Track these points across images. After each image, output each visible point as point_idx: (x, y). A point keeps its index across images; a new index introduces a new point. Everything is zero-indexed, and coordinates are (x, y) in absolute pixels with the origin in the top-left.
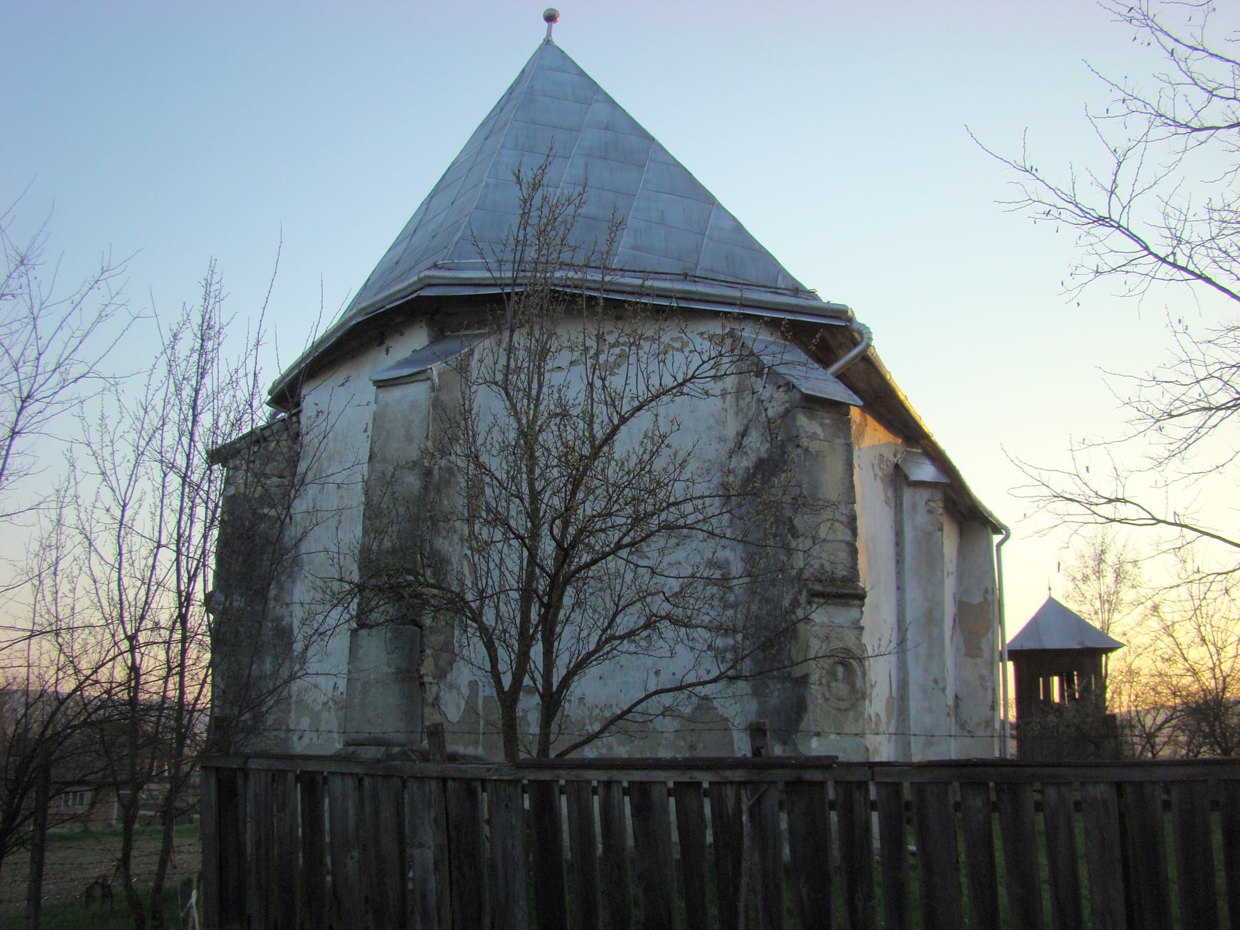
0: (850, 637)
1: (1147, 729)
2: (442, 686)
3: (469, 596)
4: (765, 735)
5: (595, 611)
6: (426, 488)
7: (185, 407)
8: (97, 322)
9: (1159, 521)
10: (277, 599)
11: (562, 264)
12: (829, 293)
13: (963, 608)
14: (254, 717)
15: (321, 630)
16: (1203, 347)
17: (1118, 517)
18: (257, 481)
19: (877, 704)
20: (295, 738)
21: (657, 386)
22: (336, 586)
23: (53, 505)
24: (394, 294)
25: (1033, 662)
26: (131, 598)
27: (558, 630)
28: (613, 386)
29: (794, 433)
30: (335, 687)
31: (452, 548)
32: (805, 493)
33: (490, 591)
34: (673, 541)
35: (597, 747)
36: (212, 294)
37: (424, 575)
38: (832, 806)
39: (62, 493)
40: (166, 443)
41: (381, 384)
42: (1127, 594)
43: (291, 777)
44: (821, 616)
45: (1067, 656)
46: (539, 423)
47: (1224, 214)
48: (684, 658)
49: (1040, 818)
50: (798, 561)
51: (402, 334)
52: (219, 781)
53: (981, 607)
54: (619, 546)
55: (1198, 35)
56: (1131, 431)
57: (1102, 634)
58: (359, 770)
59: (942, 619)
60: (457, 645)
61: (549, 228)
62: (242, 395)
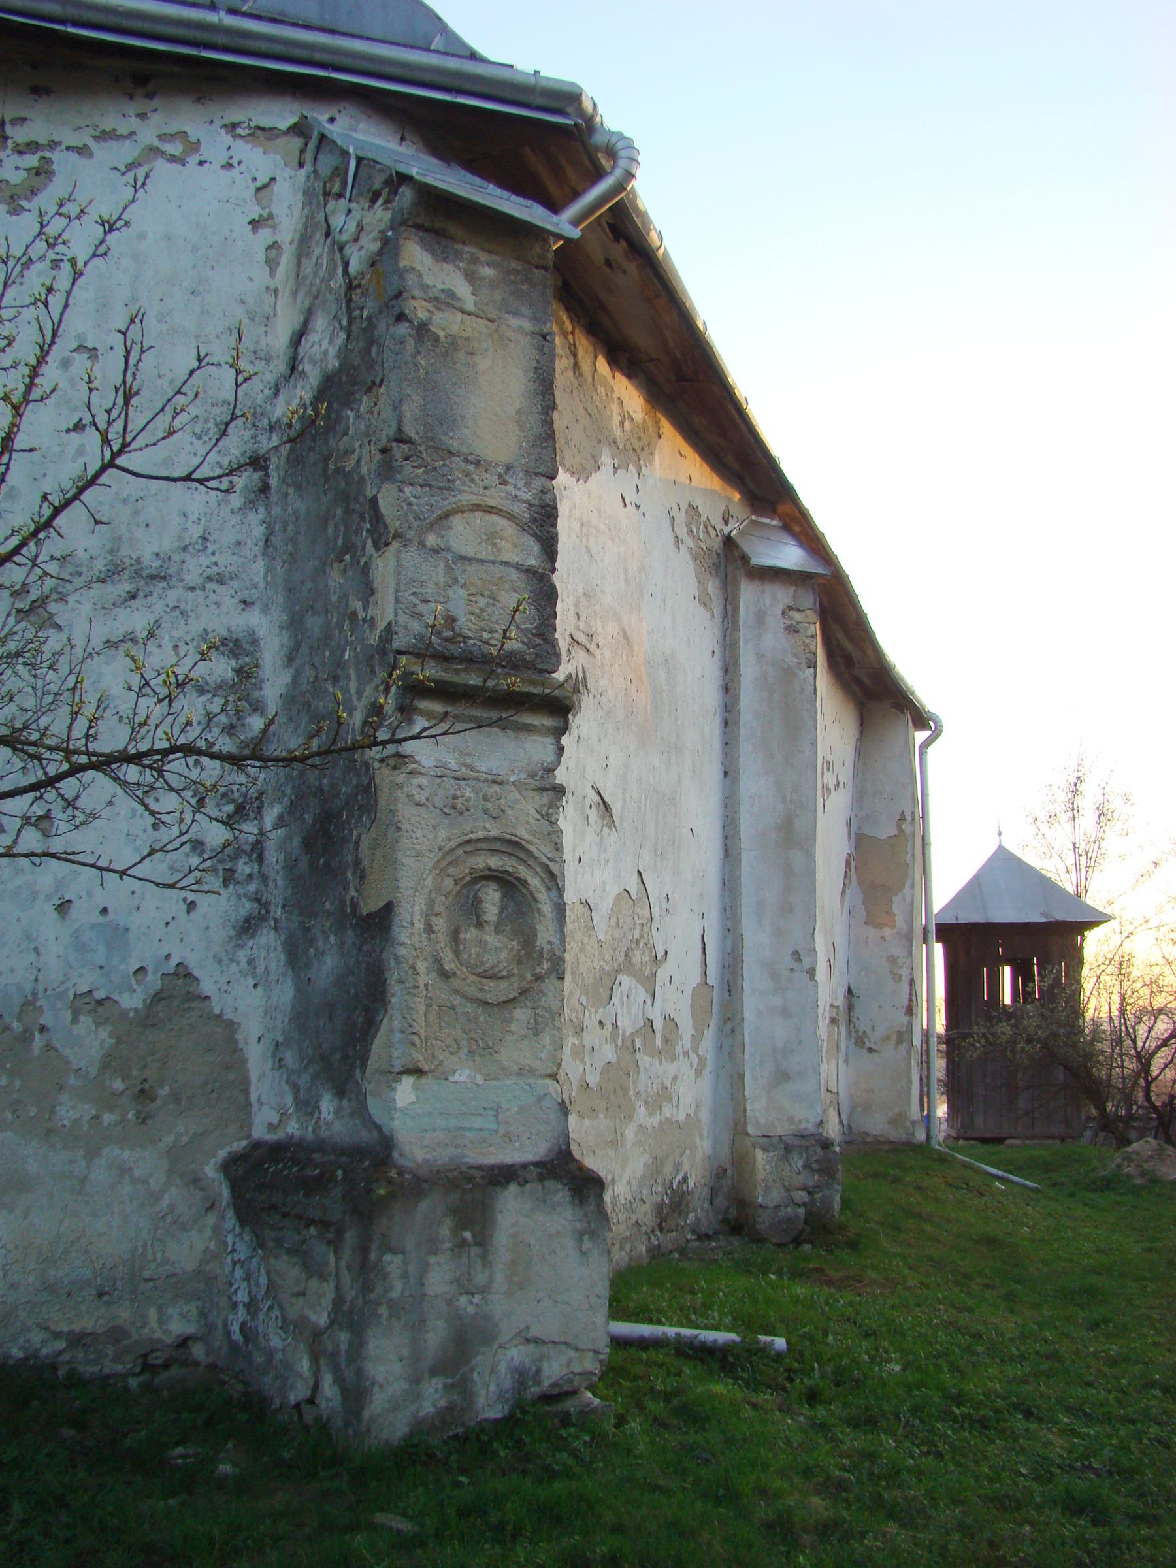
25: (972, 944)
32: (410, 431)
50: (385, 610)
53: (888, 851)
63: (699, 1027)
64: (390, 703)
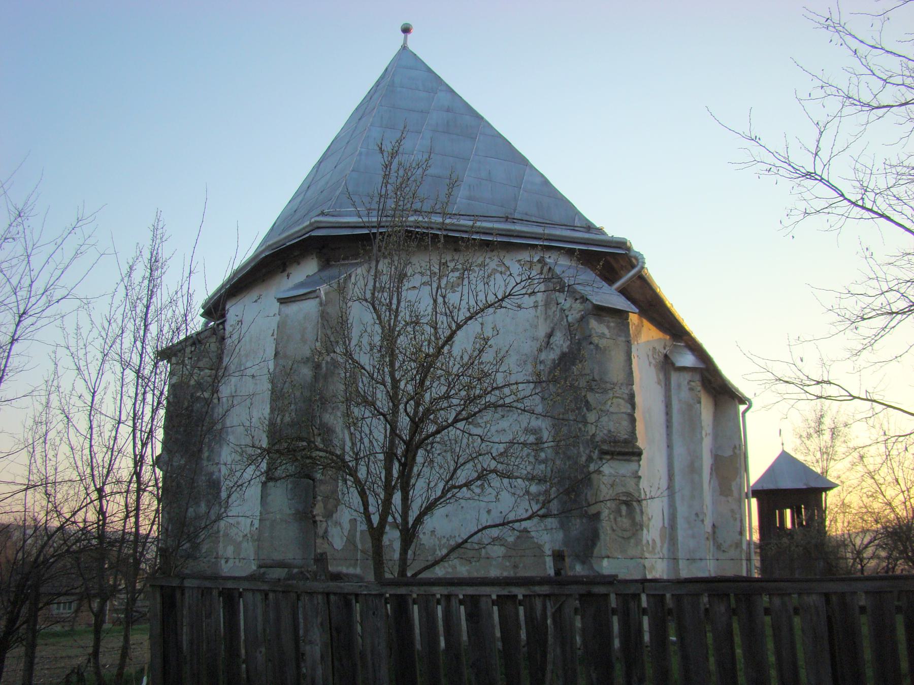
0: (631, 483)
1: (857, 547)
3: (347, 458)
4: (564, 559)
5: (441, 467)
6: (316, 378)
7: (138, 320)
8: (75, 257)
9: (855, 398)
10: (209, 459)
11: (416, 211)
12: (613, 229)
13: (718, 460)
15: (240, 482)
16: (885, 268)
17: (825, 395)
18: (194, 371)
19: (653, 532)
20: (223, 562)
21: (484, 302)
22: (250, 451)
23: (43, 393)
24: (293, 234)
25: (771, 498)
26: (100, 461)
27: (413, 481)
28: (451, 302)
30: (252, 524)
31: (335, 419)
32: (597, 378)
33: (362, 455)
35: (444, 567)
36: (159, 236)
37: (314, 442)
38: (614, 612)
39: (50, 383)
40: (124, 346)
41: (283, 301)
42: (840, 448)
43: (215, 593)
44: (610, 469)
45: (796, 495)
46: (397, 329)
47: (899, 169)
49: (768, 619)
51: (299, 264)
52: (162, 596)
53: (731, 459)
54: (456, 420)
55: (877, 38)
56: (834, 330)
57: (821, 477)
58: (265, 587)
61: (404, 186)
62: (181, 310)
63: (662, 542)
64: (595, 455)
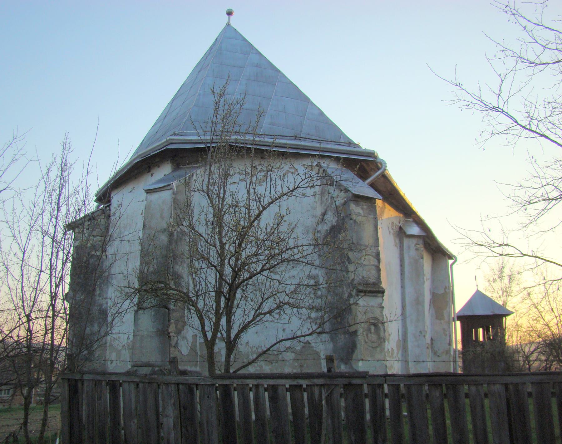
1: (526, 353)
2: (179, 338)
4: (333, 362)
5: (252, 301)
6: (170, 242)
8: (11, 163)
9: (524, 255)
10: (100, 295)
11: (236, 132)
12: (366, 145)
13: (434, 295)
14: (89, 353)
15: (120, 311)
16: (544, 170)
17: (505, 253)
18: (90, 239)
20: (109, 363)
21: (281, 192)
22: (127, 290)
25: (469, 321)
27: (234, 310)
28: (259, 192)
29: (349, 213)
30: (128, 338)
31: (182, 269)
33: (200, 293)
34: (289, 267)
35: (255, 366)
36: (67, 149)
37: (169, 284)
38: (366, 396)
40: (44, 221)
41: (148, 192)
42: (515, 288)
43: (104, 383)
44: (363, 302)
45: (485, 320)
46: (224, 210)
47: (553, 105)
48: (296, 322)
49: (467, 401)
51: (159, 167)
52: (69, 385)
53: (443, 295)
54: (262, 270)
57: (502, 307)
58: (137, 380)
59: (424, 302)
60: (186, 318)
61: (228, 116)
